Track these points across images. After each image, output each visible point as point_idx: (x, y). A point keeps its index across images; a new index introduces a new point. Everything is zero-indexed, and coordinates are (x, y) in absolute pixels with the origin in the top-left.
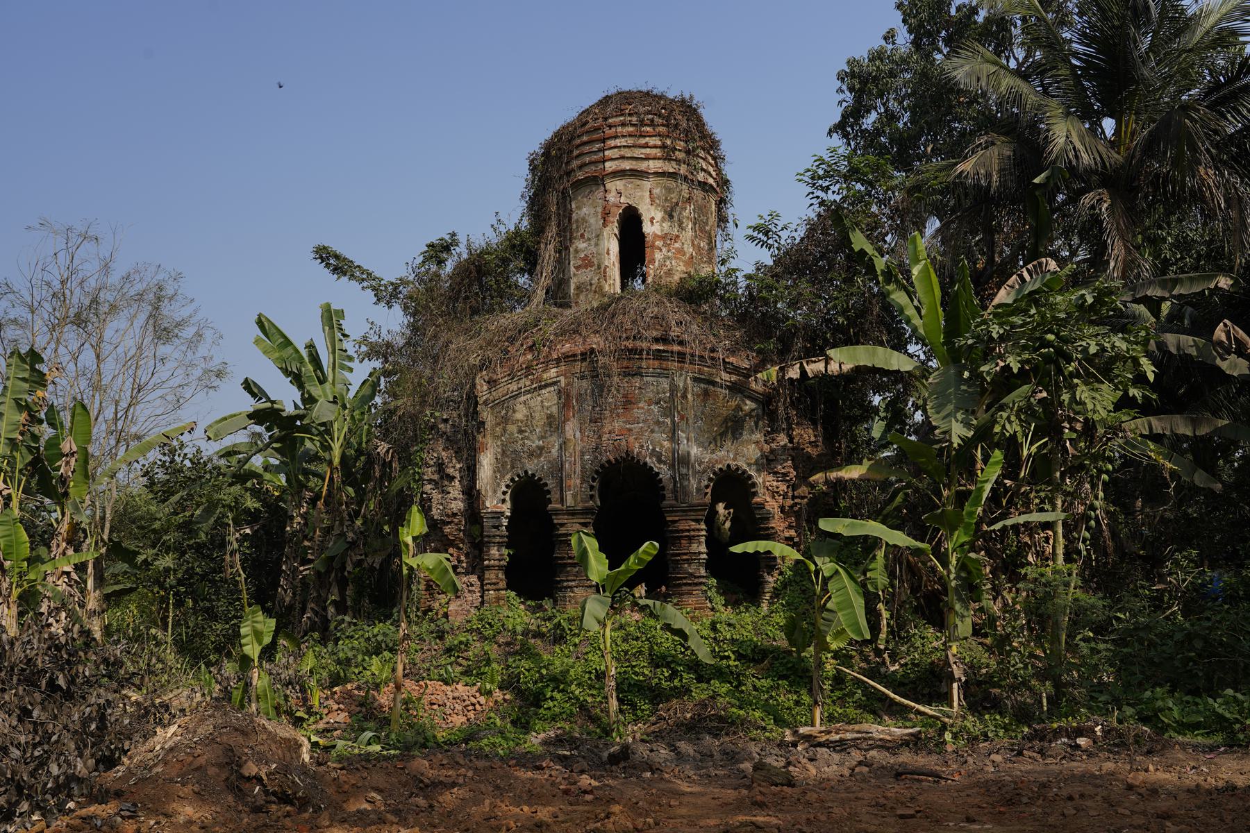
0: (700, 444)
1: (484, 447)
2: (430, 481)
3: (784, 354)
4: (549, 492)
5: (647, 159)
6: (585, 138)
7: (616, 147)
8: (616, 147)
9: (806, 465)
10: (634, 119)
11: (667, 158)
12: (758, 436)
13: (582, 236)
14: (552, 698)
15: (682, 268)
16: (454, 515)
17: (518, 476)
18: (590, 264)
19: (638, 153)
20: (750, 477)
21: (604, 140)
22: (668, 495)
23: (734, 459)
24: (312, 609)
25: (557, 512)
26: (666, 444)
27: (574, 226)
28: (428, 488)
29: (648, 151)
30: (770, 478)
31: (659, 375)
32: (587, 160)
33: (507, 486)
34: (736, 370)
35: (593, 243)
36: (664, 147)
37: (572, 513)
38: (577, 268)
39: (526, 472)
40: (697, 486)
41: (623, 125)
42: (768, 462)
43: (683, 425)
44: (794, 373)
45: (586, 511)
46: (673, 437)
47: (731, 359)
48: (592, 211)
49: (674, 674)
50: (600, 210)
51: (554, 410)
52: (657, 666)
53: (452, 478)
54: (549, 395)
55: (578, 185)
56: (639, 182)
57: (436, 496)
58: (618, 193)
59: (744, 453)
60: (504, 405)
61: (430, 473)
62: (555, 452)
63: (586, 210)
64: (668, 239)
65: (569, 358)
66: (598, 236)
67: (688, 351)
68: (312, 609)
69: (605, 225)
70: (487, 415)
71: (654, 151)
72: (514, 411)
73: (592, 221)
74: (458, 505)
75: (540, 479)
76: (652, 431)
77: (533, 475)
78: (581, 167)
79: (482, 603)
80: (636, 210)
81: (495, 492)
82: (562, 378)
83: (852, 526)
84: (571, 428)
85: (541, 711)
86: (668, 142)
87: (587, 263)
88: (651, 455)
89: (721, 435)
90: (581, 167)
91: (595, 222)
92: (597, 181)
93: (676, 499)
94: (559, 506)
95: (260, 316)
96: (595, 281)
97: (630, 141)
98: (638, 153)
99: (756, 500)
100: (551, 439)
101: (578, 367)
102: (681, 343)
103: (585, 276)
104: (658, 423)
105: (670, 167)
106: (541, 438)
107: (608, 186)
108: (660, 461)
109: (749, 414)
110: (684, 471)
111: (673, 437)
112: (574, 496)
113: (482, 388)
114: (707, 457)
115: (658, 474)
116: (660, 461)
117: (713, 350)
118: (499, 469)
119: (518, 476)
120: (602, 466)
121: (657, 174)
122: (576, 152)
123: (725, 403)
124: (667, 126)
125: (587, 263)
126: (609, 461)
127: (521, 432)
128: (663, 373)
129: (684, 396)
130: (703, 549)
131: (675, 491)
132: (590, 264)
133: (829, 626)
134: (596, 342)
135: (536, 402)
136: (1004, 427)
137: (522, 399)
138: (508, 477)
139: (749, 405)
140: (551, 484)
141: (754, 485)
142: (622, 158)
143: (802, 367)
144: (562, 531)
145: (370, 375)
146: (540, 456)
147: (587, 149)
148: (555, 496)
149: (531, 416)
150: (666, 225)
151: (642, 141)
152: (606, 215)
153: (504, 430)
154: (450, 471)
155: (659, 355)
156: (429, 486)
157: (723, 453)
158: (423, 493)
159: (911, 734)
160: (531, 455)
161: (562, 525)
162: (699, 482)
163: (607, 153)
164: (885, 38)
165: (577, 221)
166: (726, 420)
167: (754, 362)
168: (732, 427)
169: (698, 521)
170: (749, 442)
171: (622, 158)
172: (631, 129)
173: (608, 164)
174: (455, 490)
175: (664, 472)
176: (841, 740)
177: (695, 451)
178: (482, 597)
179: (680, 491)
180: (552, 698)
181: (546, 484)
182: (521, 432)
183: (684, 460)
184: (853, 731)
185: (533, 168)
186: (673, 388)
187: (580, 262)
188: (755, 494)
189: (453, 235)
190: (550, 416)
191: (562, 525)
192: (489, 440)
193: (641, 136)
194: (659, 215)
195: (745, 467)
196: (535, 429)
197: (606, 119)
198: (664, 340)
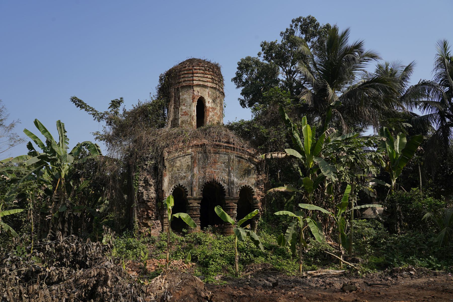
0: (237, 178)
1: (166, 175)
2: (142, 186)
3: (265, 151)
4: (187, 192)
5: (207, 82)
6: (186, 72)
7: (197, 76)
8: (197, 76)
9: (268, 186)
10: (203, 68)
11: (213, 83)
12: (255, 176)
13: (184, 104)
14: (212, 264)
15: (217, 119)
16: (152, 198)
17: (177, 186)
18: (187, 114)
19: (205, 79)
20: (252, 189)
21: (193, 73)
22: (227, 194)
23: (248, 183)
24: (51, 232)
25: (228, 199)
26: (226, 177)
27: (181, 101)
28: (141, 188)
29: (207, 79)
30: (258, 190)
31: (225, 154)
32: (187, 79)
33: (173, 189)
34: (250, 154)
35: (188, 107)
36: (212, 79)
37: (195, 199)
38: (182, 115)
39: (179, 184)
40: (236, 191)
41: (200, 69)
42: (257, 184)
43: (232, 170)
44: (269, 157)
45: (199, 199)
46: (229, 175)
47: (248, 151)
48: (188, 97)
49: (247, 254)
50: (191, 96)
51: (190, 163)
52: (241, 252)
53: (151, 185)
54: (188, 158)
55: (183, 87)
56: (205, 89)
57: (145, 192)
58: (198, 92)
59: (250, 181)
60: (173, 160)
61: (141, 183)
62: (189, 178)
63: (186, 96)
64: (214, 109)
65: (197, 146)
66: (190, 105)
67: (235, 147)
68: (51, 232)
69: (193, 102)
70: (167, 164)
71: (209, 80)
72: (176, 163)
73: (188, 100)
74: (153, 195)
75: (184, 187)
76: (222, 173)
77: (182, 186)
78: (184, 81)
79: (163, 230)
80: (203, 98)
81: (169, 191)
82: (193, 153)
83: (310, 207)
84: (196, 170)
85: (209, 269)
86: (213, 77)
87: (186, 114)
88: (222, 180)
89: (244, 175)
90: (184, 81)
91: (189, 100)
92: (191, 87)
93: (229, 195)
94: (191, 197)
95: (36, 120)
96: (189, 120)
97: (202, 75)
98: (205, 79)
99: (254, 197)
100: (188, 173)
101: (199, 149)
102: (234, 144)
103: (185, 118)
104: (224, 170)
105: (214, 86)
106: (185, 173)
107: (194, 89)
108: (224, 183)
109: (253, 168)
110: (232, 186)
111: (229, 175)
112: (196, 193)
113: (166, 155)
114: (239, 182)
115: (223, 187)
116: (224, 183)
117: (243, 147)
118: (170, 183)
119: (177, 186)
120: (205, 184)
121: (210, 87)
122: (182, 76)
123: (245, 165)
124: (213, 72)
125: (186, 114)
126: (208, 182)
127: (178, 170)
128: (227, 154)
129: (233, 162)
130: (236, 212)
131: (229, 193)
132: (187, 114)
133: (288, 238)
134: (205, 141)
135: (183, 160)
136: (345, 177)
137: (179, 159)
138: (173, 186)
139: (252, 166)
140: (188, 189)
141: (253, 192)
142: (199, 80)
143: (271, 155)
144: (191, 205)
145: (77, 145)
146: (185, 179)
147: (186, 76)
148: (189, 193)
149: (181, 165)
150: (213, 104)
151: (206, 76)
152: (193, 99)
153: (172, 169)
154: (151, 183)
155: (226, 148)
156: (141, 188)
157: (244, 181)
158: (139, 190)
159: (342, 272)
160: (182, 179)
161: (191, 203)
162: (237, 190)
163: (194, 78)
164: (258, 55)
165: (182, 99)
166: (245, 170)
167: (255, 152)
168: (247, 172)
169: (235, 203)
170: (252, 178)
171: (199, 80)
172: (202, 71)
173: (194, 82)
174: (152, 190)
175: (226, 187)
176: (321, 275)
177: (236, 180)
178: (162, 228)
179: (230, 193)
180: (212, 264)
181: (186, 189)
182: (178, 170)
183: (232, 183)
184: (324, 272)
185: (161, 80)
186: (229, 159)
187: (183, 113)
188: (254, 195)
189: (122, 98)
190: (188, 166)
191: (191, 203)
192: (167, 173)
193: (206, 74)
194: (211, 101)
195: (251, 186)
196: (182, 169)
197: (193, 67)
198: (228, 142)
